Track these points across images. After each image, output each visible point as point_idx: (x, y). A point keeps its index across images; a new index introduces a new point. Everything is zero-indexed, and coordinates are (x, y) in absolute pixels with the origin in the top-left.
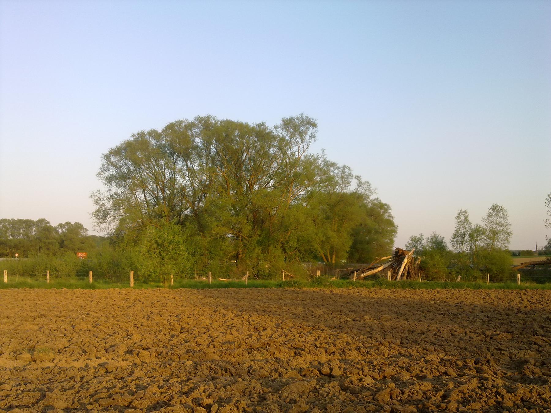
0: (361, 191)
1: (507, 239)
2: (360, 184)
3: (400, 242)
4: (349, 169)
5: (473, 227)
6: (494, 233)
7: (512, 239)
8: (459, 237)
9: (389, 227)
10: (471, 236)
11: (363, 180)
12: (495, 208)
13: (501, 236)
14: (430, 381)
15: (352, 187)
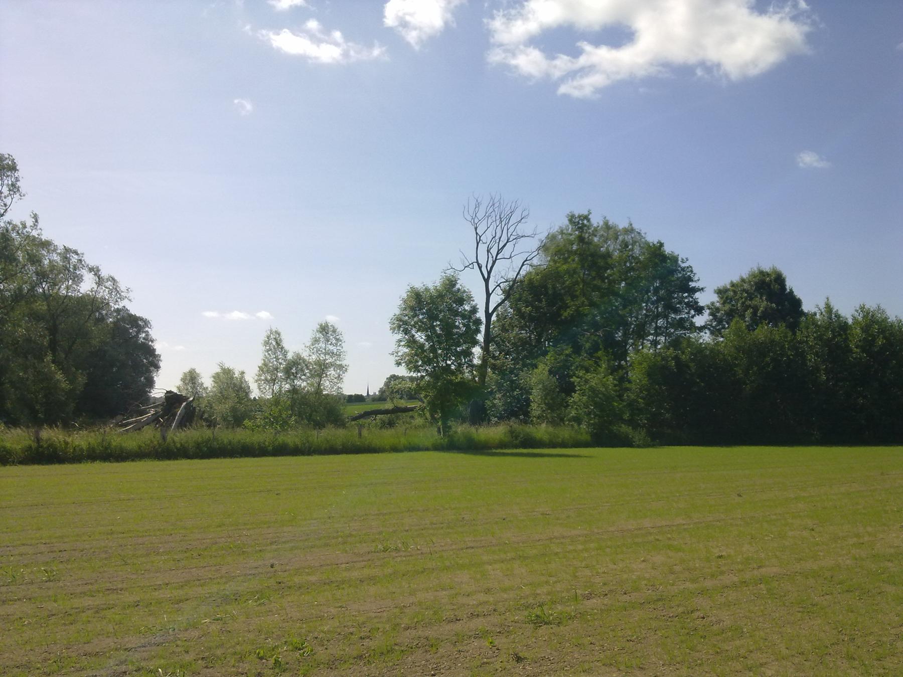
0: (103, 293)
1: (339, 378)
2: (100, 281)
3: (166, 382)
4: (76, 253)
5: (290, 356)
6: (321, 369)
7: (346, 377)
8: (268, 371)
9: (145, 359)
10: (287, 371)
11: (104, 273)
12: (324, 329)
13: (332, 372)
14: (668, 322)
15: (87, 286)
